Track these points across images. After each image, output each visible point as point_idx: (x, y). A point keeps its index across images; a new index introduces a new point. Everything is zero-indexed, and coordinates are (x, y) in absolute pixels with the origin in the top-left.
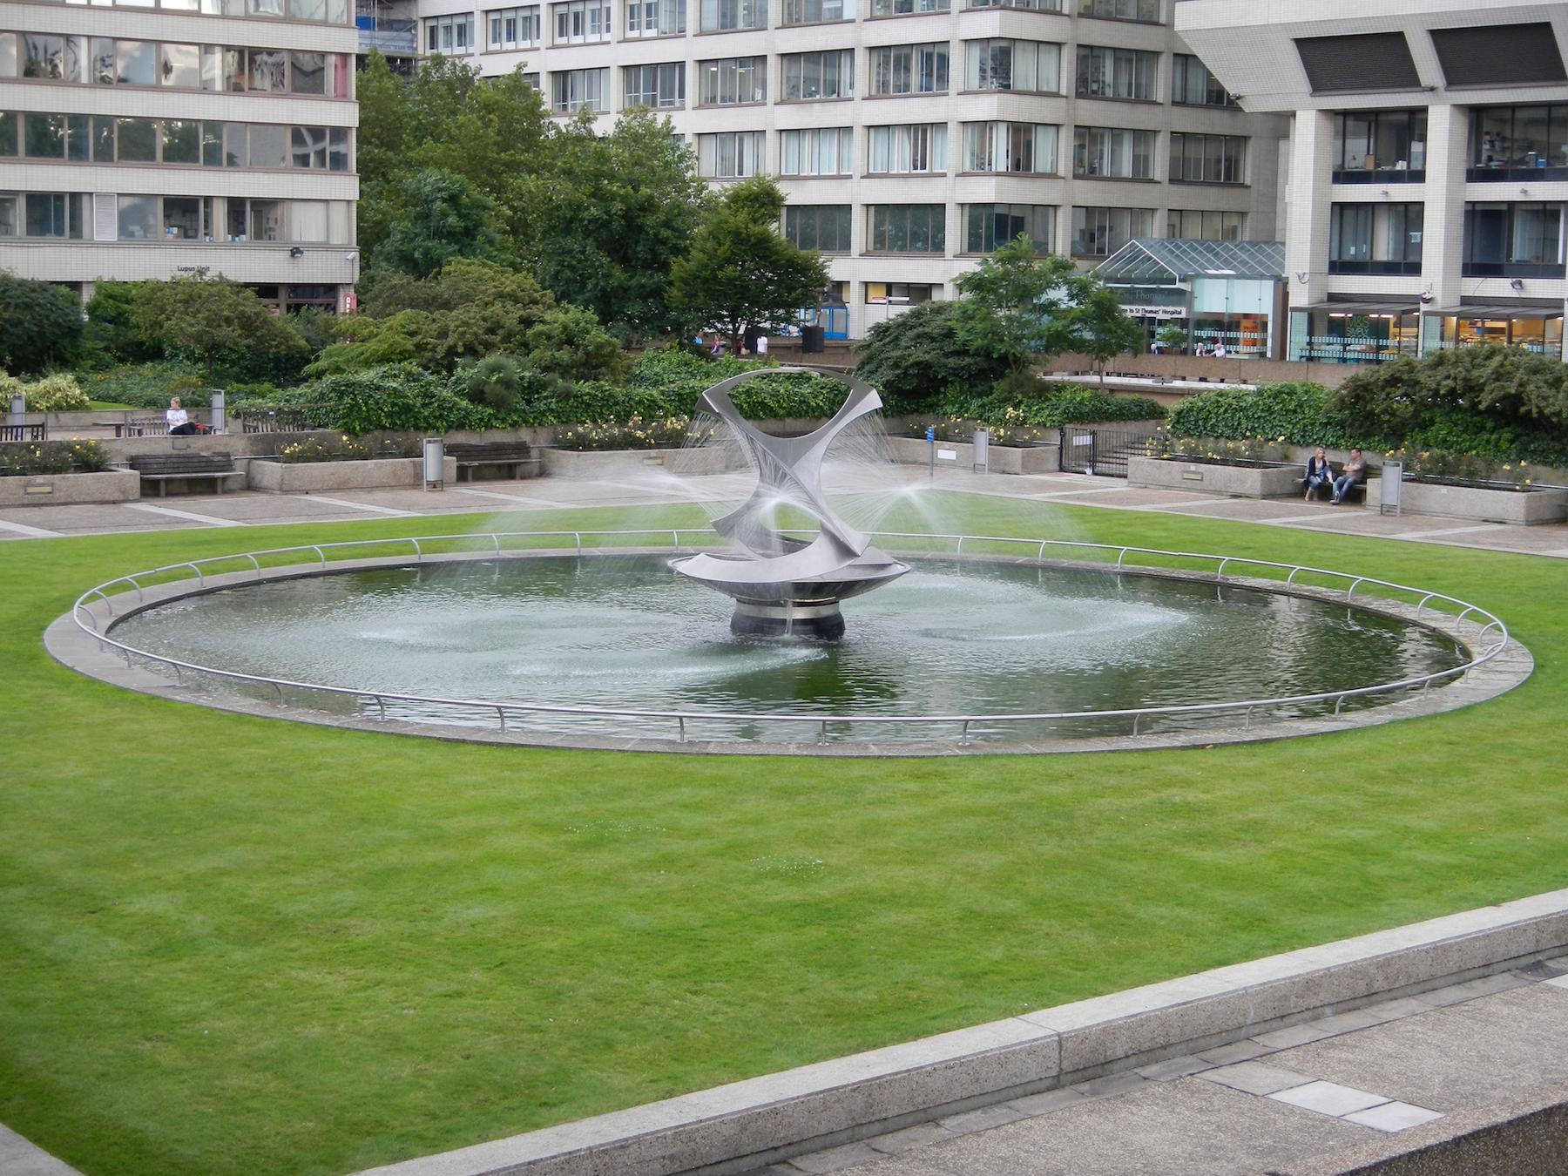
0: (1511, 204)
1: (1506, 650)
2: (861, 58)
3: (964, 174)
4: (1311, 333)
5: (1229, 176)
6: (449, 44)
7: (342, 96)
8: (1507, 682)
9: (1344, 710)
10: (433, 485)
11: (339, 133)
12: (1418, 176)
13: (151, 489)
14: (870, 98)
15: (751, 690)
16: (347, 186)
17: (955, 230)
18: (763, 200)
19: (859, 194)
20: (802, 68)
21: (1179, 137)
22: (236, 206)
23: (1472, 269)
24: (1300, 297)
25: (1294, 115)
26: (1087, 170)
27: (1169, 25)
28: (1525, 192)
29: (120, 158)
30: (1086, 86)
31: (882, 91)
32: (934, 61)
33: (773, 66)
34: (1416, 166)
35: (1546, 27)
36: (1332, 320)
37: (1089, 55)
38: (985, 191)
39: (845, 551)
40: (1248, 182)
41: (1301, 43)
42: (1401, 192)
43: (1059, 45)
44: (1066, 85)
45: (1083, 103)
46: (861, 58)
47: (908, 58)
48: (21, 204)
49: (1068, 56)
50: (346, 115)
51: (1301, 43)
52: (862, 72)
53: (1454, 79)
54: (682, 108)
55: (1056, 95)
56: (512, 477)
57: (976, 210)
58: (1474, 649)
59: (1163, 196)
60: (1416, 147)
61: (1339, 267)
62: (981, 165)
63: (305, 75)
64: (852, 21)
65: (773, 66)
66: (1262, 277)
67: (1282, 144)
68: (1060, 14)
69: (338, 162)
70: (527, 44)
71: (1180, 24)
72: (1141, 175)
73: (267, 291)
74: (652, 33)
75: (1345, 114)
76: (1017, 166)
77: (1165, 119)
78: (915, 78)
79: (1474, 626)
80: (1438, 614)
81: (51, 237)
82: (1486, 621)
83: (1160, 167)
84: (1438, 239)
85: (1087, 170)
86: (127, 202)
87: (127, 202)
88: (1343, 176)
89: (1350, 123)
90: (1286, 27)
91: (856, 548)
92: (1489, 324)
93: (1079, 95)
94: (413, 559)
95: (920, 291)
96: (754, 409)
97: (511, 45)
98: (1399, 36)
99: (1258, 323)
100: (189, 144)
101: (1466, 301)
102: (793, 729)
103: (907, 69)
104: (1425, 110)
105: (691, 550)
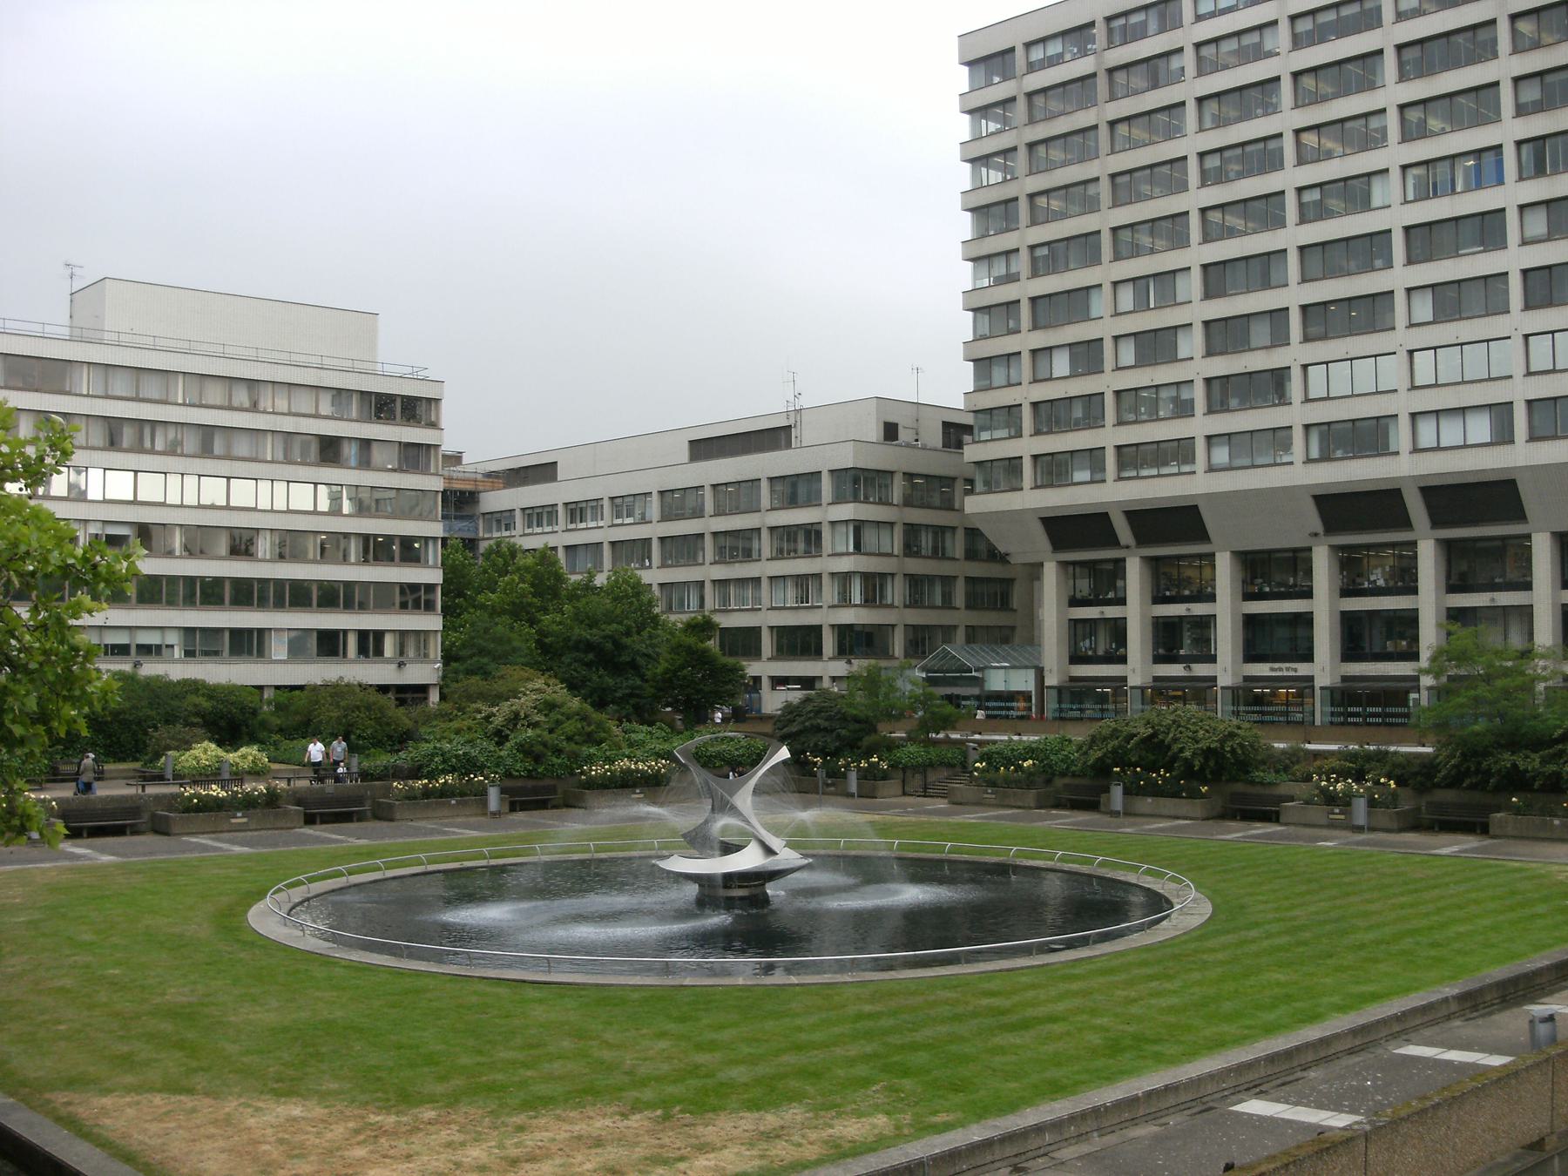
0: (1180, 617)
1: (1194, 900)
2: (765, 534)
4: (1060, 702)
6: (499, 530)
7: (435, 567)
8: (1195, 921)
9: (1095, 942)
10: (494, 814)
11: (430, 588)
12: (1122, 601)
13: (310, 820)
14: (772, 559)
15: (705, 941)
16: (432, 622)
17: (829, 643)
18: (703, 627)
19: (766, 620)
20: (728, 542)
21: (970, 580)
22: (363, 635)
23: (1158, 659)
24: (1051, 680)
26: (914, 602)
27: (962, 510)
29: (319, 605)
30: (910, 549)
31: (779, 555)
32: (812, 535)
33: (708, 540)
34: (1120, 595)
35: (1512, 484)
36: (1077, 693)
37: (912, 530)
38: (848, 616)
39: (769, 851)
42: (1111, 612)
43: (892, 524)
44: (898, 548)
46: (765, 534)
47: (796, 534)
48: (227, 635)
49: (898, 532)
50: (431, 575)
51: (946, 425)
52: (766, 544)
53: (1436, 523)
54: (650, 567)
55: (890, 555)
56: (545, 808)
57: (843, 631)
58: (1174, 900)
59: (961, 617)
60: (1119, 583)
61: (1076, 659)
62: (845, 601)
63: (409, 550)
65: (708, 540)
66: (1026, 667)
67: (1036, 583)
68: (891, 504)
69: (429, 607)
70: (593, 524)
71: (968, 510)
72: (947, 604)
73: (383, 689)
74: (630, 520)
75: (1074, 563)
76: (866, 601)
78: (801, 546)
79: (1174, 885)
80: (1149, 879)
81: (245, 657)
82: (1180, 882)
83: (959, 599)
84: (1226, 639)
85: (914, 602)
86: (293, 634)
87: (293, 634)
88: (1074, 602)
89: (1078, 570)
91: (775, 848)
92: (1172, 693)
93: (906, 555)
94: (483, 863)
95: (808, 682)
96: (705, 760)
97: (539, 530)
99: (1026, 696)
100: (332, 596)
101: (1156, 679)
102: (743, 969)
103: (795, 541)
104: (1124, 560)
105: (665, 853)
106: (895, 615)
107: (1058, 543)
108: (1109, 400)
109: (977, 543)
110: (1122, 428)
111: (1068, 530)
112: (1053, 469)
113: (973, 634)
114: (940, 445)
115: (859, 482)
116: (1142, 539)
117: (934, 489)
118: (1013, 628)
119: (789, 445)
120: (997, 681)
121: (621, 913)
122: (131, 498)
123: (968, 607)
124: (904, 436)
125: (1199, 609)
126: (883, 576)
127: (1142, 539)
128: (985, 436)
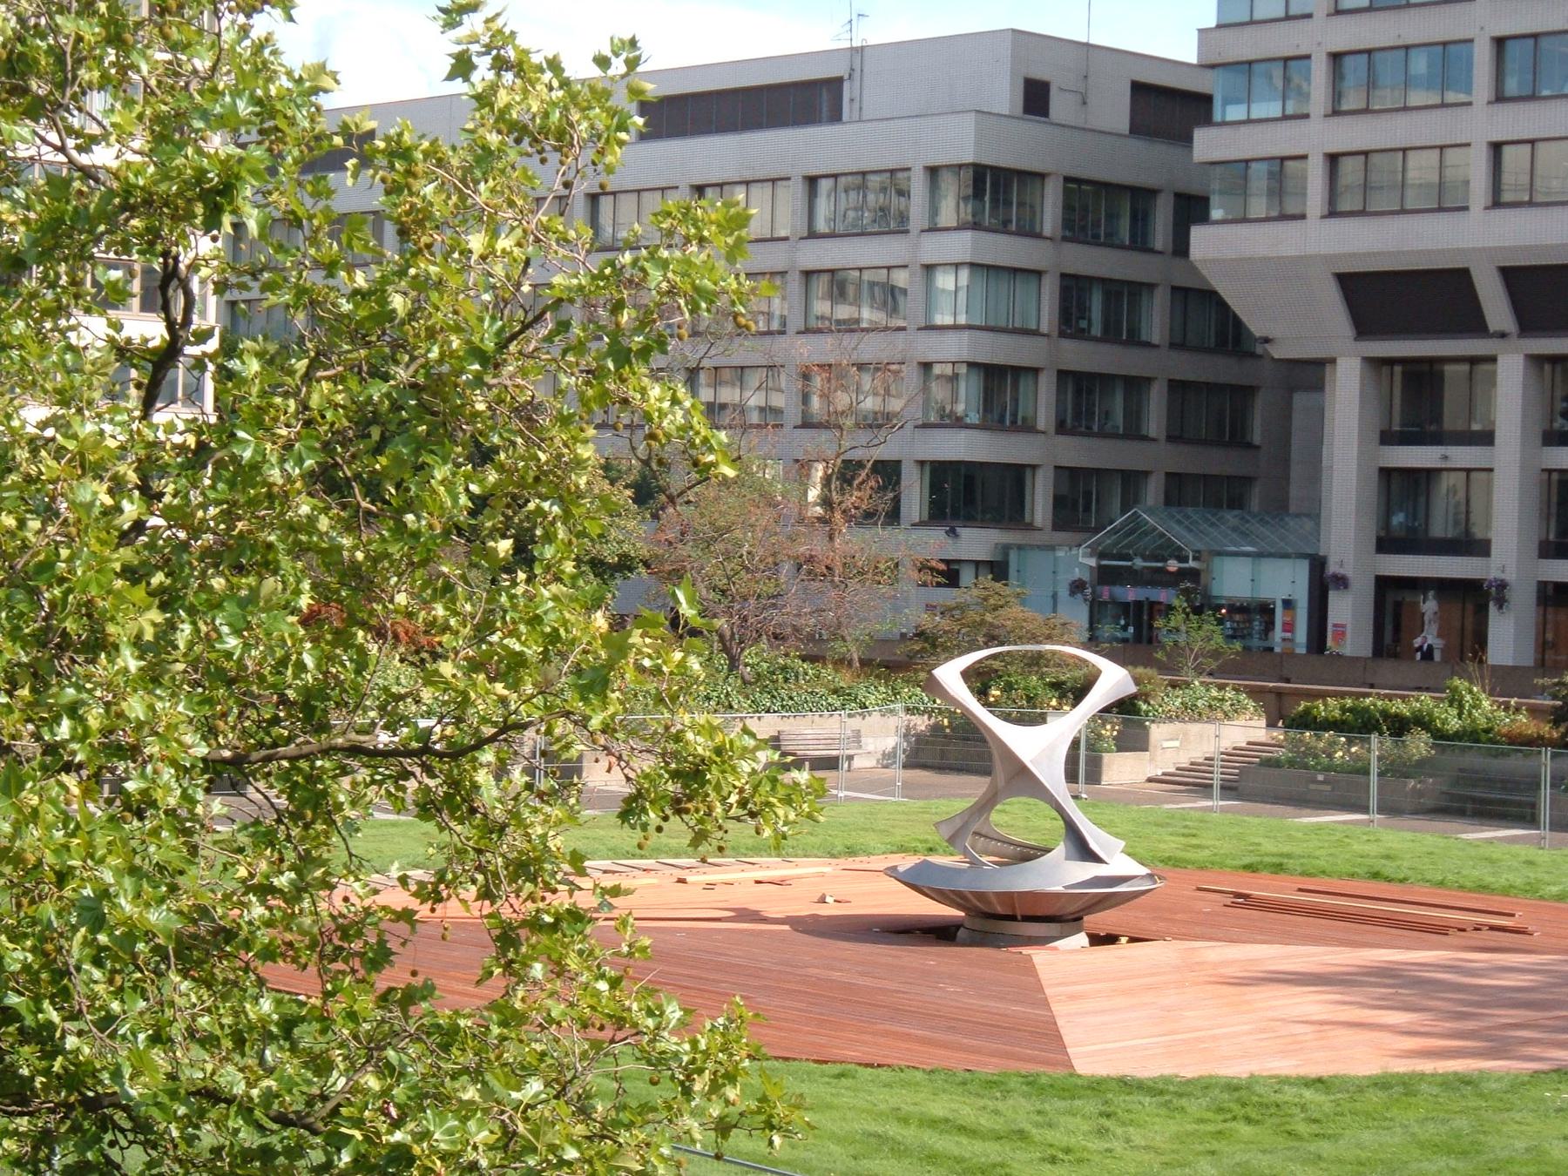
3: (925, 426)
5: (1235, 436)
21: (1178, 388)
25: (1333, 361)
28: (1445, 458)
30: (1071, 320)
37: (1074, 288)
40: (1257, 440)
41: (1139, 88)
43: (1038, 274)
45: (1067, 344)
49: (1050, 290)
51: (1139, 88)
55: (1035, 333)
57: (940, 473)
64: (786, 239)
68: (1039, 236)
72: (1133, 432)
77: (1160, 363)
83: (1155, 419)
90: (1327, 259)
93: (1062, 334)
98: (1465, 273)
106: (1042, 451)
107: (1364, 327)
108: (1483, 55)
109: (1210, 319)
110: (1336, 120)
111: (1376, 298)
112: (1353, 184)
113: (1179, 490)
114: (1124, 125)
115: (994, 190)
116: (1529, 321)
117: (1097, 206)
118: (1248, 481)
119: (836, 117)
120: (1234, 579)
121: (964, 1128)
122: (1247, 19)
123: (1061, 428)
124: (1060, 106)
125: (1462, 456)
126: (1017, 371)
127: (1529, 321)
128: (1235, 112)
